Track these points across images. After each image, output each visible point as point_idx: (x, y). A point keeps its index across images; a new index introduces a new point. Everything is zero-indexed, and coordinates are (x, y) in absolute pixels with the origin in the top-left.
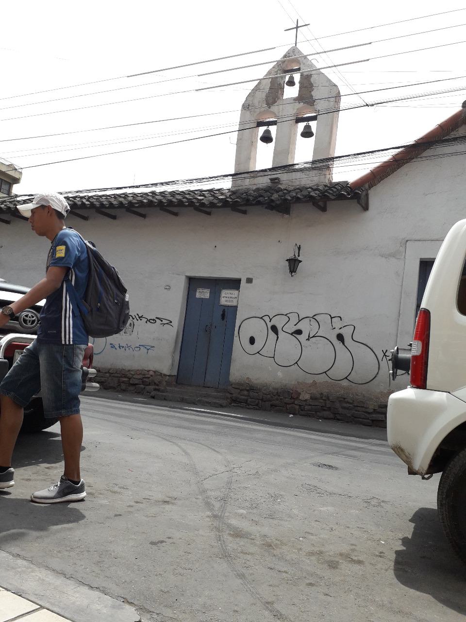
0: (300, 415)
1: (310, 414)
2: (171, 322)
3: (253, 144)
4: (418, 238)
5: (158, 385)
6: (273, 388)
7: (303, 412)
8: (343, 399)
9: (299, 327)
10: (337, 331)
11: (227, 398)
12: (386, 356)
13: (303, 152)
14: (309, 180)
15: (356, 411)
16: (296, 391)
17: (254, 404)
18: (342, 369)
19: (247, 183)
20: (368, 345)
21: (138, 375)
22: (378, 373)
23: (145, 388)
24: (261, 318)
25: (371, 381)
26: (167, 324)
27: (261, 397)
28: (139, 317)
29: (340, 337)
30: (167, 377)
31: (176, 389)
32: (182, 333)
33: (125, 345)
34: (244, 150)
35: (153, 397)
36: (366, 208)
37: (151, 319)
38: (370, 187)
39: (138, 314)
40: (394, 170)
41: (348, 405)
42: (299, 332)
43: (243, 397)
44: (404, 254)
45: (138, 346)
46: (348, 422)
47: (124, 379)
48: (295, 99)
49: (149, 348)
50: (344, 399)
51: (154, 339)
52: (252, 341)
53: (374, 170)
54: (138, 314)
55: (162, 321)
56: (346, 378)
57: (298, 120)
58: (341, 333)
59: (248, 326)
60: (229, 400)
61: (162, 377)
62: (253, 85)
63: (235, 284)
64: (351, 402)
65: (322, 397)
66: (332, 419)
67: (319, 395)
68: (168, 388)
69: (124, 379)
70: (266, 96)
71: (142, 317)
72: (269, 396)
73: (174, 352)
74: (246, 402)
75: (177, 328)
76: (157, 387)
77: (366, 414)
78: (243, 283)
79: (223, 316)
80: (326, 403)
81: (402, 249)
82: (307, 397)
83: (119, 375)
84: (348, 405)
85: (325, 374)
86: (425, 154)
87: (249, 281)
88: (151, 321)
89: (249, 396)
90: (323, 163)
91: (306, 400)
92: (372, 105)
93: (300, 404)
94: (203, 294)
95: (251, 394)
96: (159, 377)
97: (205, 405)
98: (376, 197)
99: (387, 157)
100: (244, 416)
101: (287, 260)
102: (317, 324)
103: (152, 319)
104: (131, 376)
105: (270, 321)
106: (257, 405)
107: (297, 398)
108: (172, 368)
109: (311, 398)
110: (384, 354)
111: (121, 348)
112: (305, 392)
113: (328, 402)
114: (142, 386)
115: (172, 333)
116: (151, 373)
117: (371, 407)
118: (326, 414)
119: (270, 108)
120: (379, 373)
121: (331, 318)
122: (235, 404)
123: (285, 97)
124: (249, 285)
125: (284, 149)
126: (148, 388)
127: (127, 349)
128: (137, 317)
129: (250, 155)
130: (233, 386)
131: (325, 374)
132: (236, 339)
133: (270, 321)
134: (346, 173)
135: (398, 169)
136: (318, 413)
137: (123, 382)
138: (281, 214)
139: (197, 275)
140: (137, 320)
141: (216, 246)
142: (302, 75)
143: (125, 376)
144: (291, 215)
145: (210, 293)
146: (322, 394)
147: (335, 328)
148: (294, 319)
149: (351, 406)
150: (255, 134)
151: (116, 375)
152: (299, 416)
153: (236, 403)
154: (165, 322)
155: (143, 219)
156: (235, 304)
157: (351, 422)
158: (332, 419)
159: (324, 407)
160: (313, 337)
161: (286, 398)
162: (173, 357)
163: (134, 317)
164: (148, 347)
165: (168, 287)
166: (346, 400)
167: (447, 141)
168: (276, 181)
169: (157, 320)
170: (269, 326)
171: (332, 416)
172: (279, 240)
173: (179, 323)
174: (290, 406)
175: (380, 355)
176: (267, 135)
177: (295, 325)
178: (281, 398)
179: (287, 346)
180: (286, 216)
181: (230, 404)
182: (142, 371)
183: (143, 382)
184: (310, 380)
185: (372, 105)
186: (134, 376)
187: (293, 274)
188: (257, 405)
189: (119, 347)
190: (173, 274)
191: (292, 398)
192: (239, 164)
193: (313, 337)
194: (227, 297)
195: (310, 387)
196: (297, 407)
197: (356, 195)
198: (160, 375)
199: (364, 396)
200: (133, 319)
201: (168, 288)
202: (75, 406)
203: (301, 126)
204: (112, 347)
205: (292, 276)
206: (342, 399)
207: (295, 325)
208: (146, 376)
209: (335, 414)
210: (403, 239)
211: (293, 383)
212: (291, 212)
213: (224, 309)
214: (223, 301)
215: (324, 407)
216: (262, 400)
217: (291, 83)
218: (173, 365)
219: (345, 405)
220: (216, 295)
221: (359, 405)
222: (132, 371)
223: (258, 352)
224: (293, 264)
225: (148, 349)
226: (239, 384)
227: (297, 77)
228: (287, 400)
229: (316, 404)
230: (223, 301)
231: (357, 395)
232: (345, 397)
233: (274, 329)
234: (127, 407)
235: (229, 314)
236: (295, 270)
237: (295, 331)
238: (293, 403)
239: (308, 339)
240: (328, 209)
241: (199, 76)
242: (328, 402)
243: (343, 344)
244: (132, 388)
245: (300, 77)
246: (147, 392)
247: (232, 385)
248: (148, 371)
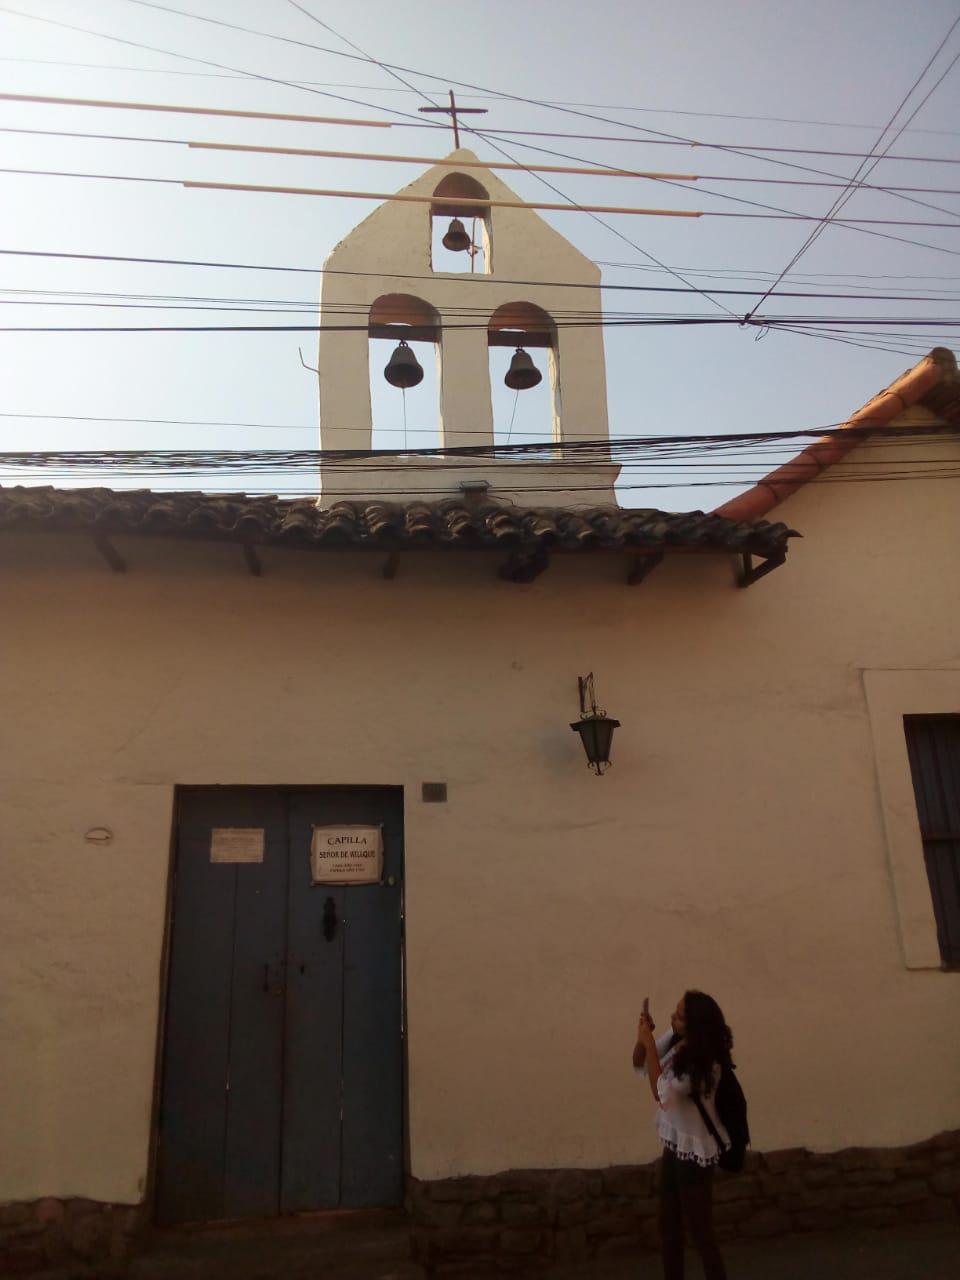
87: (435, 793)
94: (238, 846)
165: (101, 834)
197: (739, 545)
214: (325, 868)
220: (289, 851)
224: (596, 735)
230: (325, 868)
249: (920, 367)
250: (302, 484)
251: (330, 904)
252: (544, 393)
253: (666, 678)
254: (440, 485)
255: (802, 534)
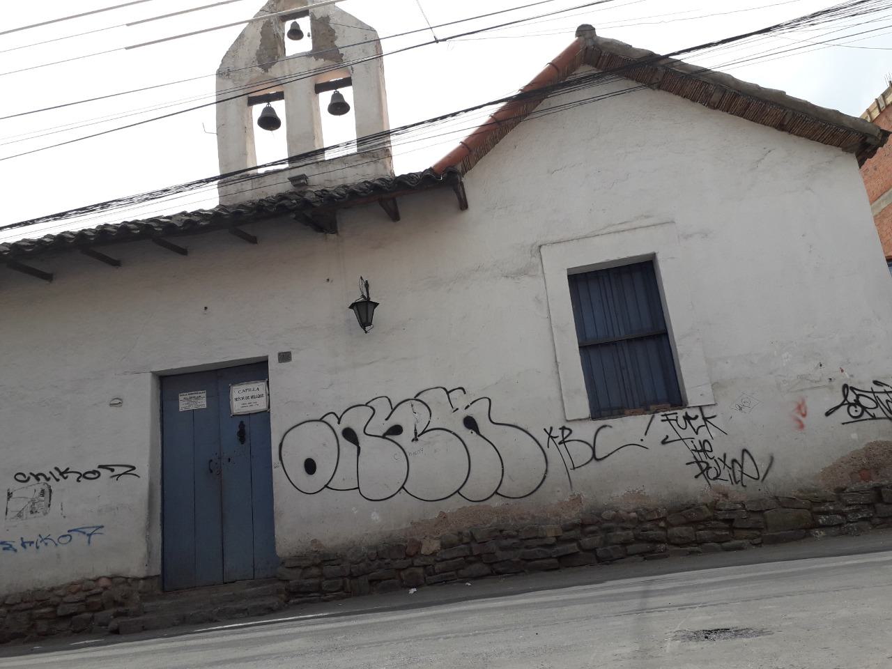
0: (429, 585)
1: (446, 577)
2: (134, 468)
3: (246, 131)
4: (555, 239)
5: (122, 604)
6: (370, 548)
7: (433, 578)
8: (498, 534)
9: (394, 421)
10: (463, 413)
11: (279, 592)
12: (552, 437)
13: (338, 134)
14: (355, 176)
15: (527, 547)
16: (413, 540)
17: (337, 589)
18: (485, 479)
19: (248, 193)
20: (519, 425)
21: (74, 593)
22: (547, 471)
23: (93, 617)
24: (321, 420)
25: (538, 487)
26: (125, 473)
27: (347, 572)
28: (61, 474)
29: (470, 423)
30: (142, 582)
31: (165, 602)
32: (159, 487)
33: (34, 538)
34: (231, 137)
35: (116, 632)
36: (463, 205)
37: (86, 473)
38: (466, 169)
39: (57, 469)
40: (495, 141)
41: (510, 541)
42: (397, 430)
43: (311, 581)
44: (540, 267)
45: (67, 533)
46: (516, 573)
47: (43, 611)
48: (308, 55)
49: (89, 533)
50: (501, 531)
51: (100, 511)
52: (310, 467)
53: (466, 140)
54: (57, 469)
55: (113, 470)
56: (496, 492)
57: (320, 88)
58: (469, 415)
59: (295, 441)
60: (283, 596)
61: (130, 585)
62: (238, 30)
63: (256, 369)
64: (515, 533)
65: (461, 540)
66: (488, 575)
67: (457, 538)
68: (146, 605)
69: (43, 611)
70: (256, 54)
71: (67, 471)
72: (362, 565)
73: (149, 527)
74: (319, 589)
75: (147, 477)
76: (121, 609)
77: (546, 550)
78: (273, 364)
79: (242, 435)
80: (471, 550)
81: (536, 260)
82: (435, 545)
83: (29, 605)
84: (510, 541)
85: (457, 493)
86: (539, 107)
87: (285, 357)
88: (88, 475)
89: (322, 575)
90: (374, 142)
91: (434, 554)
92: (444, 40)
93: (425, 563)
94: (193, 401)
95: (328, 570)
96: (121, 586)
97: (235, 618)
98: (475, 185)
99: (483, 117)
100: (342, 612)
101: (351, 307)
102: (426, 408)
103: (91, 470)
104: (57, 599)
105: (339, 423)
106: (342, 589)
107: (418, 553)
108: (149, 561)
109: (443, 546)
110: (549, 435)
111: (27, 545)
112: (428, 538)
113: (474, 545)
114: (87, 615)
115: (138, 490)
116: (104, 582)
117: (551, 534)
118: (477, 568)
119: (266, 71)
120: (549, 469)
121: (448, 393)
122: (297, 600)
123: (288, 54)
124: (285, 365)
125: (305, 128)
126: (100, 616)
127: (42, 545)
128: (57, 474)
129: (245, 148)
130: (287, 564)
131: (457, 493)
132: (277, 472)
133: (339, 423)
134: (412, 157)
135: (500, 139)
136: (461, 572)
137: (41, 618)
138: (321, 234)
139: (175, 367)
140: (58, 480)
141: (206, 308)
142: (313, 19)
143: (44, 603)
144: (340, 233)
145: (207, 397)
146: (460, 533)
147: (457, 409)
148: (383, 409)
149: (515, 541)
150: (248, 116)
151: (23, 606)
152: (428, 587)
153: (296, 598)
154: (118, 470)
155: (48, 282)
156: (261, 405)
157: (523, 571)
158: (488, 575)
159: (468, 556)
160: (424, 432)
161: (396, 559)
162: (148, 539)
163: (48, 475)
164: (90, 531)
165: (118, 401)
166: (504, 532)
167: (569, 84)
168: (302, 181)
169: (100, 470)
170: (339, 429)
171: (486, 570)
172: (327, 278)
173: (152, 471)
174: (408, 572)
175: (543, 439)
176: (269, 114)
177: (387, 419)
178: (387, 561)
179: (380, 460)
180: (332, 237)
181: (287, 602)
182: (81, 582)
183: (87, 606)
184: (432, 512)
185: (444, 40)
186: (65, 599)
187: (367, 328)
188: (342, 589)
189: (23, 545)
190: (125, 373)
191: (408, 556)
192: (226, 166)
193: (424, 432)
194: (244, 398)
195: (436, 525)
196: (420, 571)
197: (445, 183)
198: (123, 583)
199: (533, 517)
200: (48, 479)
201: (117, 403)
202: (865, 121)
203: (326, 98)
204: (4, 549)
205: (366, 332)
206: (499, 533)
207: (387, 419)
208: (94, 591)
209: (491, 564)
210: (532, 246)
211: (404, 526)
212: (339, 230)
213: (242, 422)
214: (237, 407)
215: (468, 556)
216: (351, 576)
217: (296, 34)
218: (149, 553)
219: (505, 543)
220: (220, 399)
221: (529, 537)
222: (59, 588)
223: (326, 486)
224: (364, 310)
225: (89, 535)
226: (300, 557)
227: (305, 24)
228: (399, 563)
229: (455, 555)
230: (237, 407)
231: (522, 519)
232: (502, 528)
233: (349, 434)
234: (554, 598)
235: (253, 429)
236: (370, 321)
237: (388, 431)
238: (412, 565)
239: (415, 439)
240: (401, 215)
241: (127, 48)
242: (474, 545)
243: (478, 432)
244: (63, 625)
245: (309, 21)
246: (101, 624)
247: (283, 563)
248: (97, 580)
249: (570, 39)
250: (208, 199)
251: (242, 425)
252: (350, 117)
253: (400, 271)
254: (283, 186)
255: (863, 167)
